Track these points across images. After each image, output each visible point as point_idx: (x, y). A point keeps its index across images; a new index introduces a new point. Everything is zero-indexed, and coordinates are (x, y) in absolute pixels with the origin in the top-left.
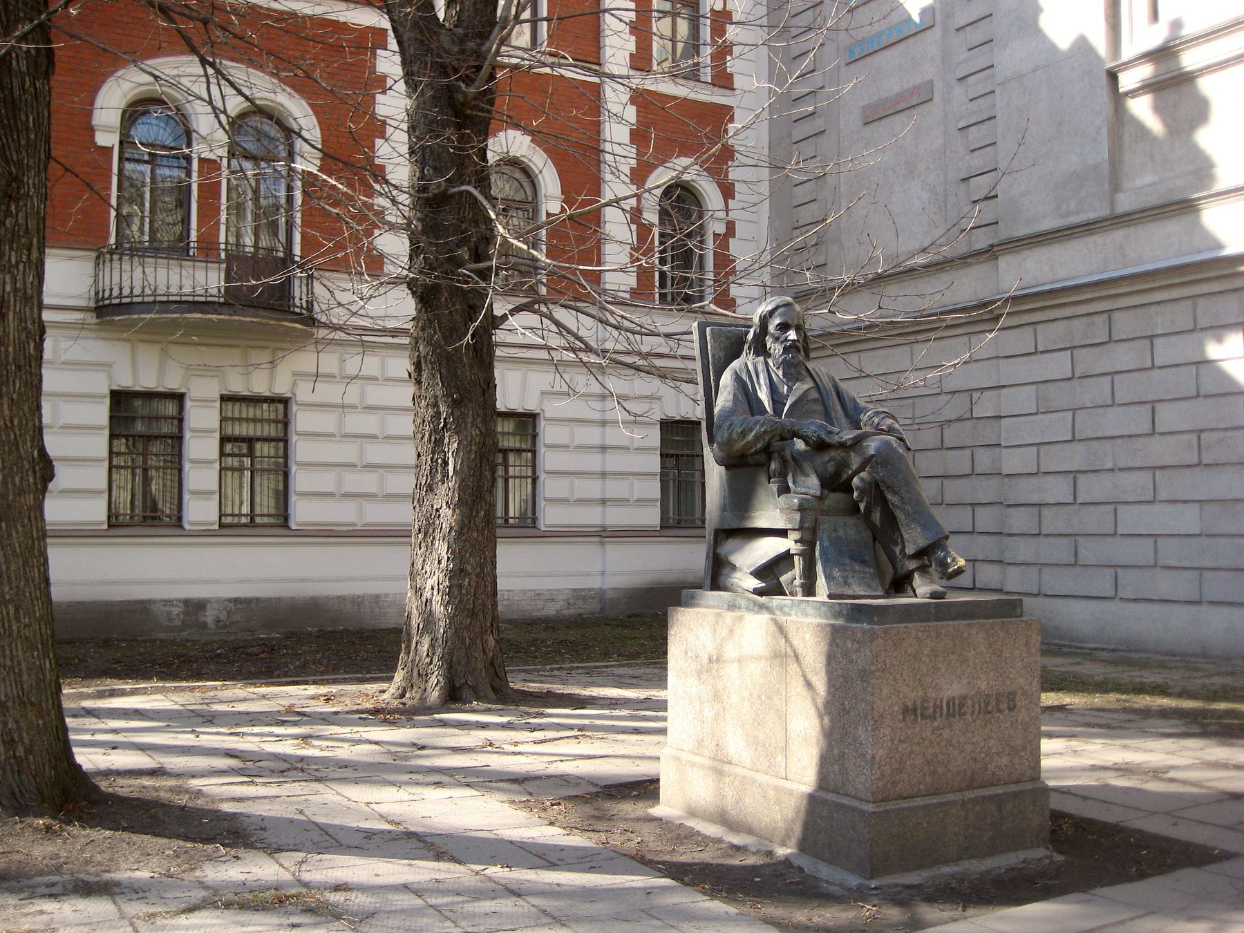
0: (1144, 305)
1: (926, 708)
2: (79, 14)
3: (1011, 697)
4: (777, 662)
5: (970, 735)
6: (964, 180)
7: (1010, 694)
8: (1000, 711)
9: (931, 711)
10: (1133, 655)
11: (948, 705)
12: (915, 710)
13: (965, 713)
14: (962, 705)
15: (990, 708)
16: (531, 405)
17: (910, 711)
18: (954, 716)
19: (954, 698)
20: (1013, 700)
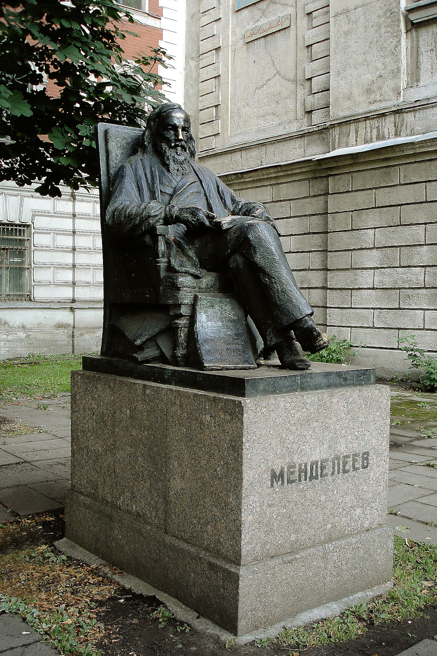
0: (82, 308)
1: (292, 473)
2: (75, 104)
3: (366, 456)
4: (306, 115)
5: (330, 493)
6: (308, 47)
7: (364, 453)
8: (355, 469)
9: (297, 474)
10: (274, 182)
11: (312, 469)
12: (282, 475)
13: (327, 475)
14: (323, 468)
15: (347, 467)
16: (26, 219)
17: (276, 477)
18: (317, 478)
19: (317, 462)
20: (367, 459)
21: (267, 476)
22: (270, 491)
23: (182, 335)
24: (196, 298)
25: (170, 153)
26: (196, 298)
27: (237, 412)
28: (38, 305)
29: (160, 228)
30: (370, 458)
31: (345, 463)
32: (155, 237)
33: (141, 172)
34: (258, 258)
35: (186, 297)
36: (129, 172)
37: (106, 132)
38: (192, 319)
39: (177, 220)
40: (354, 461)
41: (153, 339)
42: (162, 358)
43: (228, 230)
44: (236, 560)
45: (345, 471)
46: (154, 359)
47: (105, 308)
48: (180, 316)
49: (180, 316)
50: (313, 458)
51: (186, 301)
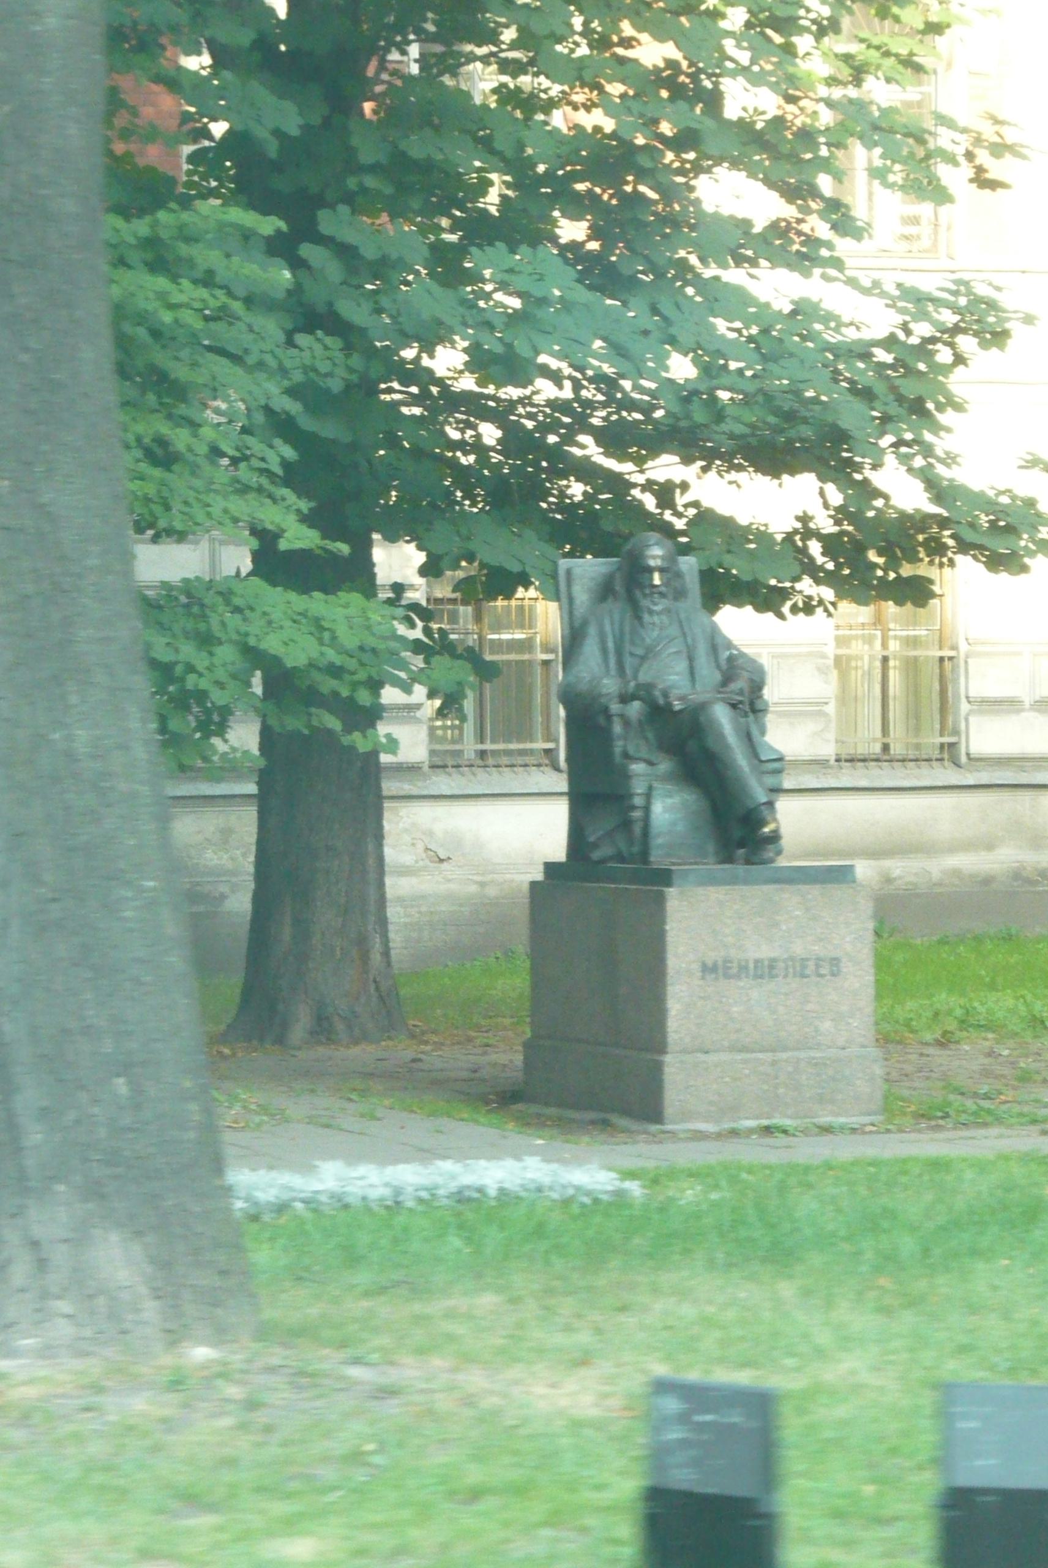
3: (835, 961)
17: (708, 969)
21: (696, 967)
22: (701, 982)
23: (637, 829)
24: (650, 788)
25: (645, 603)
26: (650, 788)
27: (660, 900)
28: (984, 778)
29: (615, 707)
30: (842, 965)
31: (804, 967)
32: (609, 717)
33: (608, 628)
34: (710, 743)
35: (639, 788)
36: (592, 630)
37: (569, 572)
38: (647, 809)
39: (634, 697)
40: (818, 966)
41: (609, 834)
42: (620, 858)
43: (681, 711)
44: (661, 1048)
45: (803, 976)
46: (611, 858)
47: (263, 800)
48: (634, 808)
49: (634, 808)
50: (758, 956)
51: (639, 791)
